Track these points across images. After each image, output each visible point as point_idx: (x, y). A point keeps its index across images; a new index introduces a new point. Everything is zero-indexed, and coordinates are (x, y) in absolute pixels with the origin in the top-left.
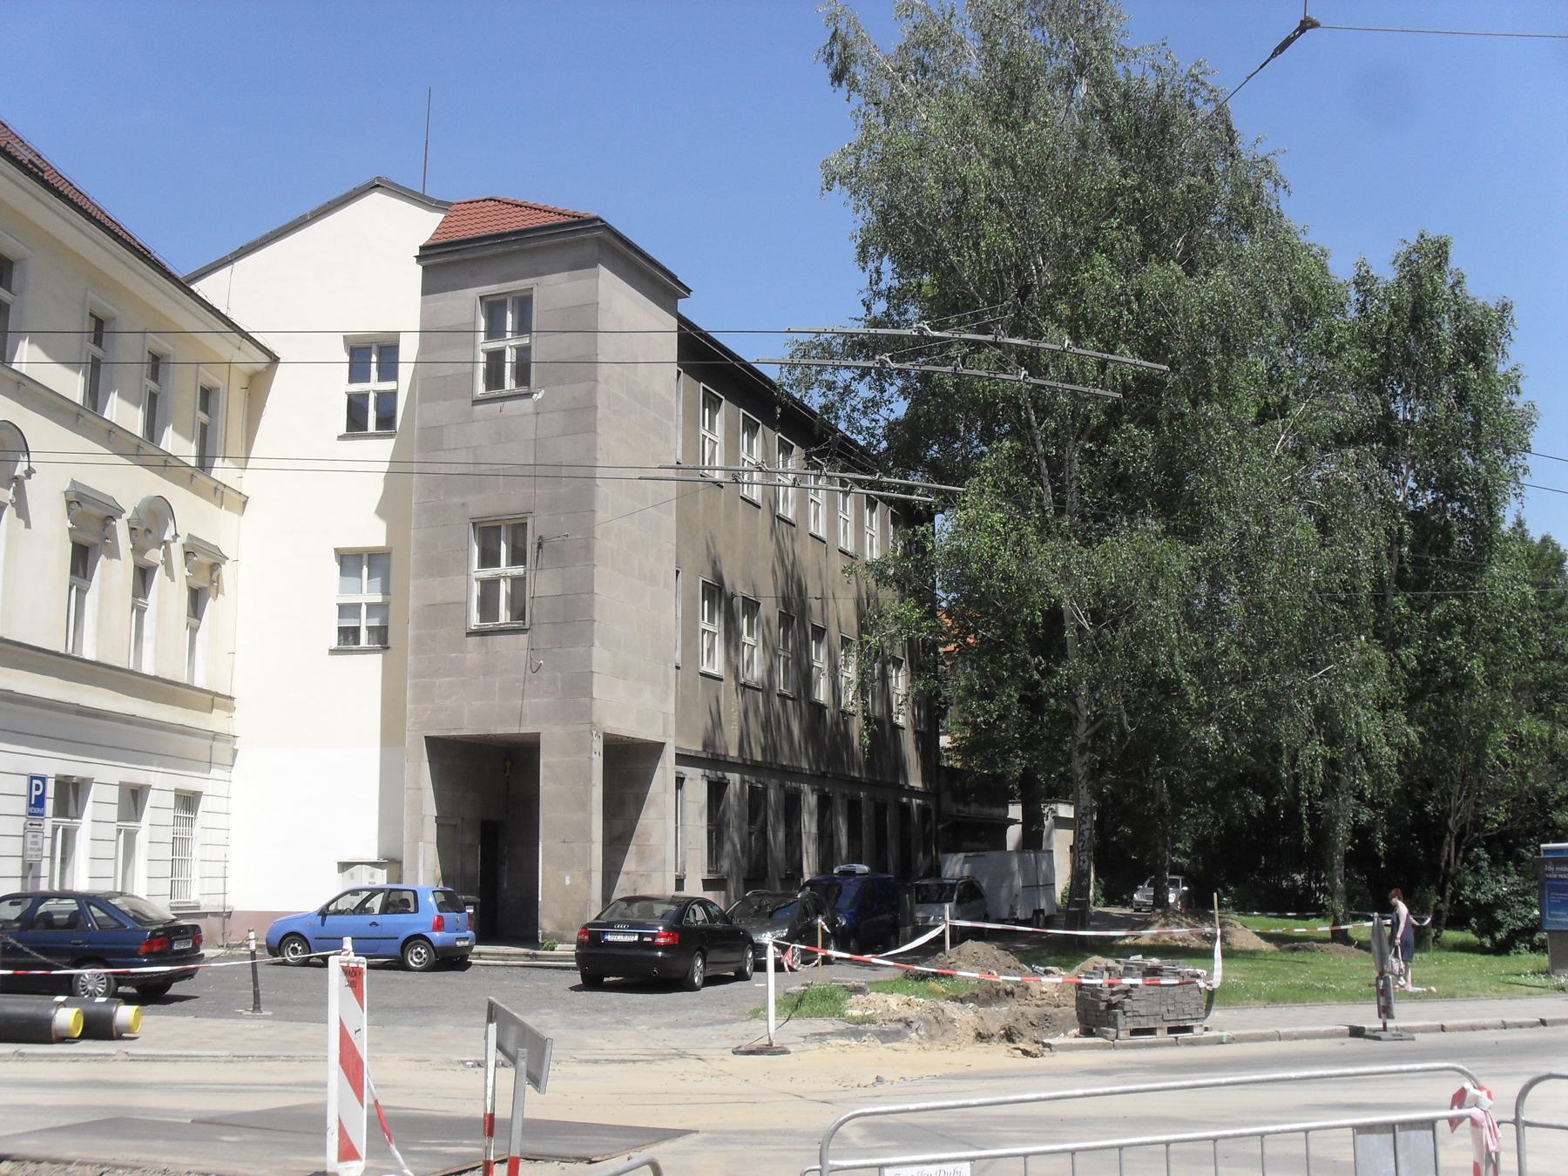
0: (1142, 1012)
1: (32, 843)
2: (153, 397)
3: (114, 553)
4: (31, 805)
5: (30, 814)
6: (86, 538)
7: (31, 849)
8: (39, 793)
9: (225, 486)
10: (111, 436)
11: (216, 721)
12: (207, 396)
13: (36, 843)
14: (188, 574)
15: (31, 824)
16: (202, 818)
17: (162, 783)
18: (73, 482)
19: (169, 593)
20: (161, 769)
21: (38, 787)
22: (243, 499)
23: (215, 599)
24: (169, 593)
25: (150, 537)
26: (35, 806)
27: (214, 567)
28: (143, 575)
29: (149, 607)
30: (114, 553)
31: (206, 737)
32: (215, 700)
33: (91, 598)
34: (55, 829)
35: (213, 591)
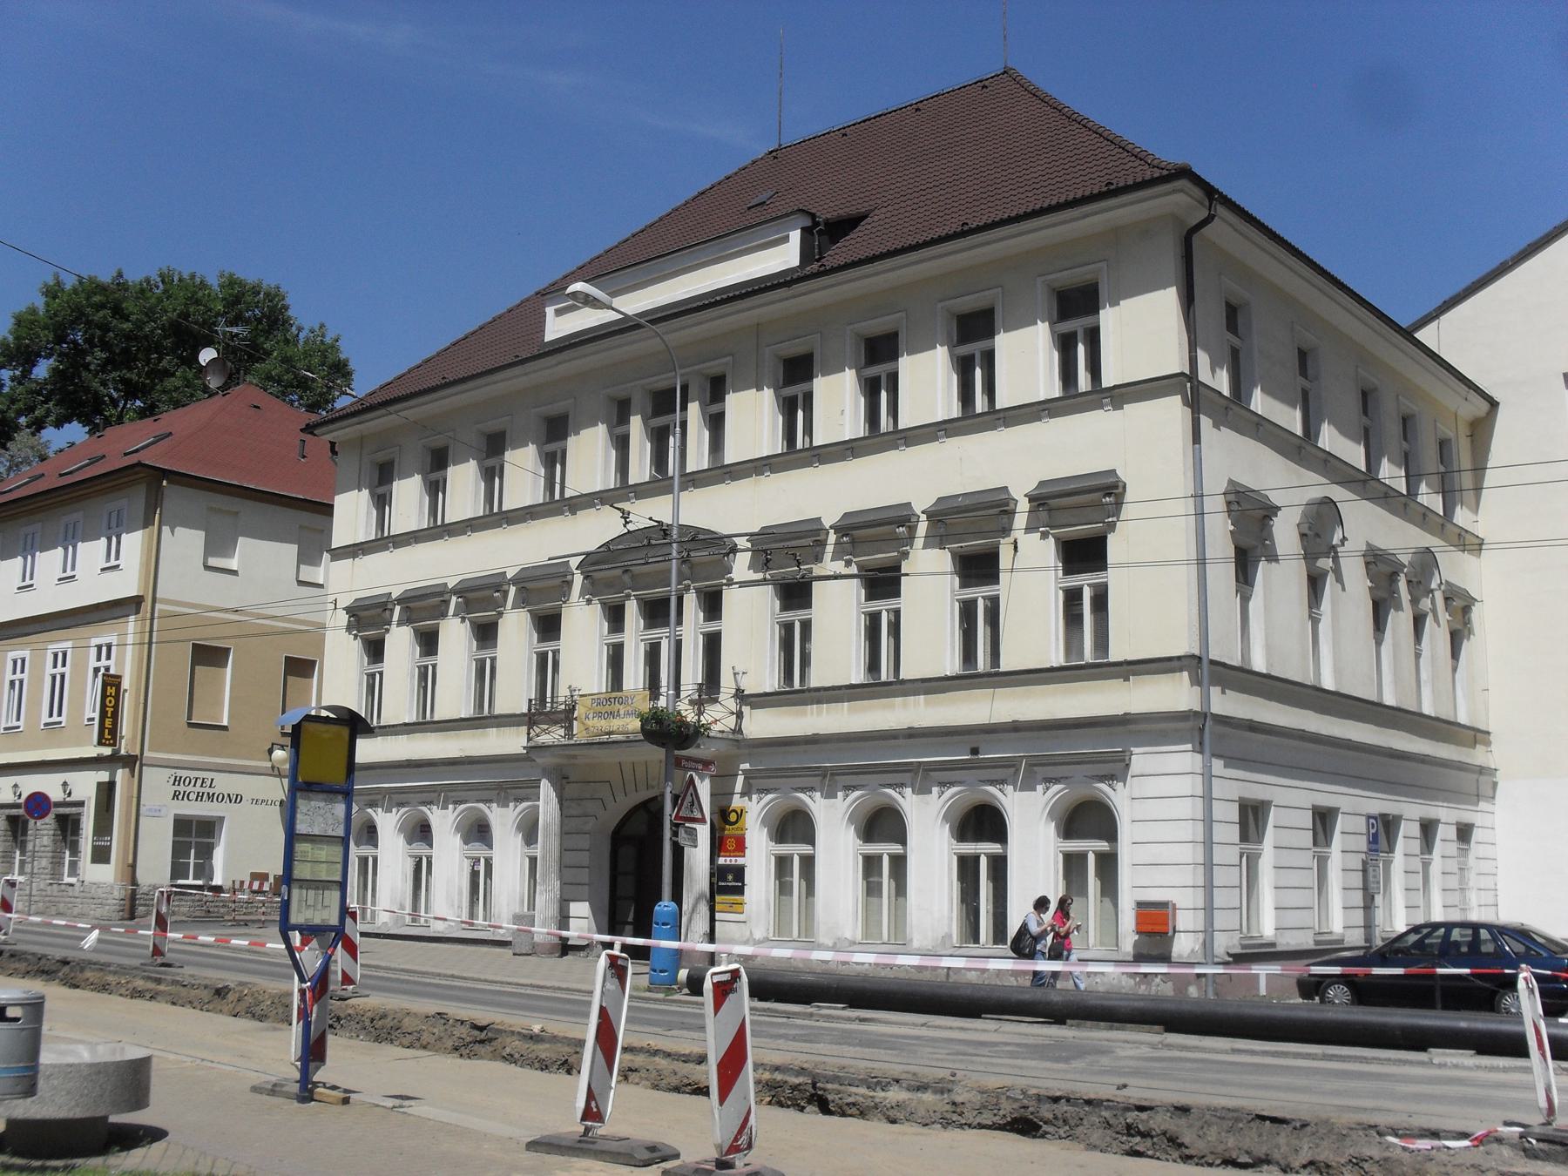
2: (1305, 395)
3: (1399, 607)
4: (1370, 842)
5: (1370, 850)
6: (1247, 542)
9: (1466, 531)
10: (1261, 430)
11: (1478, 756)
12: (1444, 445)
14: (1450, 618)
16: (1475, 849)
17: (1447, 815)
18: (1231, 482)
19: (1437, 635)
20: (1445, 804)
21: (1373, 824)
23: (1469, 639)
24: (1437, 635)
25: (1421, 587)
27: (1466, 610)
28: (1418, 622)
29: (1423, 653)
30: (1399, 607)
31: (1473, 772)
32: (1477, 736)
33: (1255, 604)
35: (1466, 632)
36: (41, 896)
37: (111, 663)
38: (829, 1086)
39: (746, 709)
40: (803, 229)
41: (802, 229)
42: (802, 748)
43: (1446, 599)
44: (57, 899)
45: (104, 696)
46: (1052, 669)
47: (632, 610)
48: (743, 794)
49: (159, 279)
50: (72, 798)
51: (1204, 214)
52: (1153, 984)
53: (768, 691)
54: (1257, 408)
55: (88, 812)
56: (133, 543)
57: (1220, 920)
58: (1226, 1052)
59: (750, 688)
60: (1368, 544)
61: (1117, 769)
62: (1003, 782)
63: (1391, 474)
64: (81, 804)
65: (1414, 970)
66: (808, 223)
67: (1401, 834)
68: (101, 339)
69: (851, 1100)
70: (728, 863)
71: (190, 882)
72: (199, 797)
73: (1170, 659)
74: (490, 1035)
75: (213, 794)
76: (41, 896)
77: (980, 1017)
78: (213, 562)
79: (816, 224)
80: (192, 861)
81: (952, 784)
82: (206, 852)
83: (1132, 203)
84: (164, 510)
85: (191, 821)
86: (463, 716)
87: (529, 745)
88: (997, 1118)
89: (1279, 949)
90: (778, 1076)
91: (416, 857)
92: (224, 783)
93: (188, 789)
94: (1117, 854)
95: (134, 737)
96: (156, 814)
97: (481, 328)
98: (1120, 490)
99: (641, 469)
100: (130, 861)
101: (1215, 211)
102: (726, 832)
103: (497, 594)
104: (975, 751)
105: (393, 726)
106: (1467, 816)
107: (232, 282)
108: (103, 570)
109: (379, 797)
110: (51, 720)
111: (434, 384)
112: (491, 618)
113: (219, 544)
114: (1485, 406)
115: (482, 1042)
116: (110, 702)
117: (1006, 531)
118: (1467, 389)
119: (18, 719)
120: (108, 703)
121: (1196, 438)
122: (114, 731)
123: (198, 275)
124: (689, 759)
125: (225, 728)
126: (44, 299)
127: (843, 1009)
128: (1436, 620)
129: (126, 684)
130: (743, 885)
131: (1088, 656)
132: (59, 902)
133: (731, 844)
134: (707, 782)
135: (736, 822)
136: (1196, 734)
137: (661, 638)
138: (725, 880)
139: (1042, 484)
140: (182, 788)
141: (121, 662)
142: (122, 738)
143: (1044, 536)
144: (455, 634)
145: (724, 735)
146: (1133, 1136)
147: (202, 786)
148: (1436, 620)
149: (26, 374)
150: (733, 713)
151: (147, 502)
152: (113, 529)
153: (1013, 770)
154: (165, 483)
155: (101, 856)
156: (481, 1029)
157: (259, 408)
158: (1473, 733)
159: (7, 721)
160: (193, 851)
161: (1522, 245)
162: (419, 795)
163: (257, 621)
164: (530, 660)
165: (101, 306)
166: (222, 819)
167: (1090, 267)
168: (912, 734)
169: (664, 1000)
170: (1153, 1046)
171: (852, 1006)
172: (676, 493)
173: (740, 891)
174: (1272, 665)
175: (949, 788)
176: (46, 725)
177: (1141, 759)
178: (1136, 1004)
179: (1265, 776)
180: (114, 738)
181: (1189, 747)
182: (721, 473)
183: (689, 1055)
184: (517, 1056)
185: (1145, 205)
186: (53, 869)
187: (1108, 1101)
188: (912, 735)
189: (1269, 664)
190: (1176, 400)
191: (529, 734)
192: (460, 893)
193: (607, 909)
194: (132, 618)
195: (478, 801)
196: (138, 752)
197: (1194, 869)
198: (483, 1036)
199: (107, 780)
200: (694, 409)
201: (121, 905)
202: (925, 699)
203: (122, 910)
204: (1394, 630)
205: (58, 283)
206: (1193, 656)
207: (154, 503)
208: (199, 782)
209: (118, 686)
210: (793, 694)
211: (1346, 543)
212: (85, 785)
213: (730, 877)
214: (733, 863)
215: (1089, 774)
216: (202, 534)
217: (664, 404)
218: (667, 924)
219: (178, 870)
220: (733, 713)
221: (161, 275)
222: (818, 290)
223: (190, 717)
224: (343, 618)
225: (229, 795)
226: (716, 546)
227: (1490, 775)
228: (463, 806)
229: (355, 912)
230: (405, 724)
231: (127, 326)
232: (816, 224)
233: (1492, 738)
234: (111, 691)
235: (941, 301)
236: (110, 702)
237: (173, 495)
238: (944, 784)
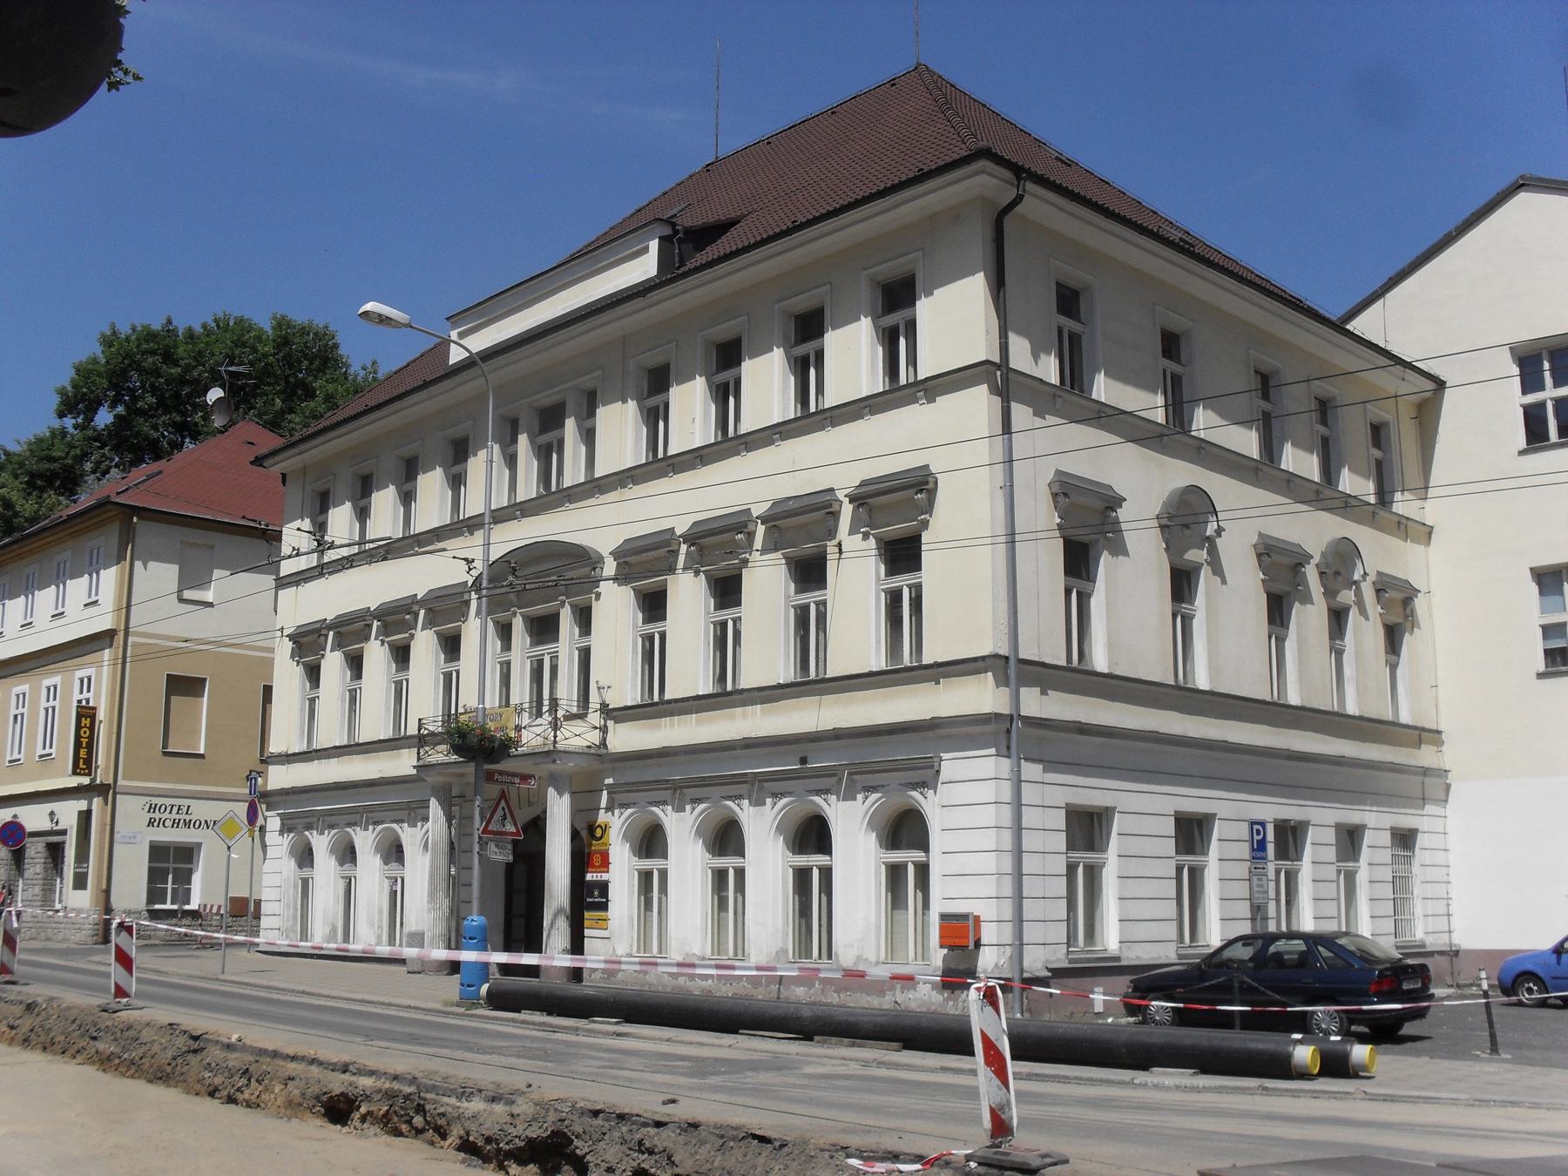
3: (1307, 599)
4: (1253, 850)
5: (1253, 858)
7: (1258, 892)
8: (1260, 837)
9: (1408, 519)
11: (1426, 756)
13: (1262, 886)
14: (1381, 611)
16: (1420, 856)
17: (1377, 822)
19: (1365, 632)
22: (1428, 530)
23: (1412, 633)
24: (1365, 632)
28: (1338, 618)
30: (1307, 599)
31: (1416, 774)
34: (1278, 872)
35: (1408, 625)
36: (34, 922)
37: (90, 695)
38: (429, 1096)
39: (610, 723)
40: (661, 238)
41: (660, 238)
42: (656, 761)
43: (1378, 591)
44: (46, 925)
45: (78, 727)
46: (871, 674)
47: (518, 625)
48: (608, 809)
49: (214, 325)
50: (60, 827)
51: (1013, 194)
52: (960, 1000)
53: (629, 704)
54: (1099, 395)
55: (71, 840)
56: (110, 577)
57: (1031, 933)
58: (933, 1070)
59: (615, 702)
60: (1260, 535)
61: (927, 777)
62: (827, 791)
63: (1299, 461)
64: (64, 832)
66: (667, 231)
68: (152, 385)
69: (441, 1110)
70: (595, 879)
71: (168, 906)
72: (175, 823)
73: (975, 660)
74: (202, 1044)
75: (190, 821)
76: (34, 922)
77: (737, 1033)
78: (188, 594)
79: (676, 232)
80: (169, 886)
81: (783, 795)
82: (184, 878)
83: (940, 188)
84: (136, 547)
85: (169, 848)
86: (382, 738)
87: (419, 764)
88: (542, 1130)
89: (1123, 963)
90: (396, 1086)
91: (390, 878)
92: (201, 810)
93: (164, 816)
94: (929, 865)
95: (107, 767)
96: (131, 840)
97: (422, 355)
98: (931, 486)
99: (528, 488)
100: (104, 887)
101: (1024, 191)
102: (593, 848)
103: (408, 617)
104: (803, 761)
105: (326, 749)
106: (1406, 820)
107: (281, 324)
108: (85, 605)
109: (314, 819)
110: (44, 752)
111: (355, 413)
112: (404, 641)
113: (193, 578)
114: (1430, 385)
115: (195, 1051)
116: (85, 733)
117: (832, 533)
118: (1403, 369)
119: (20, 753)
121: (1007, 428)
122: (88, 761)
124: (501, 773)
125: (202, 756)
126: (102, 348)
127: (617, 1023)
128: (1363, 611)
129: (101, 715)
130: (608, 901)
131: (907, 660)
132: (47, 928)
133: (597, 860)
134: (566, 798)
135: (601, 837)
136: (1003, 737)
137: (544, 655)
138: (592, 896)
139: (863, 484)
140: (157, 815)
141: (97, 696)
142: (97, 767)
143: (866, 536)
144: (376, 654)
145: (592, 751)
146: (643, 1153)
147: (178, 813)
148: (1363, 611)
149: (89, 420)
150: (596, 728)
151: (120, 537)
152: (93, 567)
153: (835, 779)
154: (135, 519)
155: (80, 882)
156: (196, 1038)
157: (253, 444)
158: (1417, 732)
159: (12, 753)
160: (170, 876)
161: (1467, 214)
162: (345, 817)
163: (218, 649)
164: (437, 680)
165: (153, 353)
166: (199, 845)
167: (905, 258)
168: (749, 744)
169: (463, 1015)
170: (866, 1063)
171: (628, 1021)
172: (487, 511)
173: (604, 907)
174: (1117, 664)
175: (781, 799)
176: (41, 756)
177: (952, 765)
178: (879, 1019)
180: (89, 767)
181: (993, 751)
182: (596, 486)
183: (336, 1064)
184: (213, 1065)
185: (952, 189)
186: (44, 895)
187: (638, 1115)
188: (749, 745)
189: (1111, 660)
190: (983, 389)
191: (418, 753)
192: (380, 911)
193: (502, 927)
194: (107, 650)
195: (392, 822)
196: (111, 781)
197: (998, 879)
198: (196, 1046)
199: (85, 809)
200: (570, 424)
201: (95, 930)
202: (762, 710)
203: (97, 935)
204: (1298, 624)
205: (114, 333)
206: (996, 656)
207: (128, 536)
208: (175, 809)
209: (93, 718)
210: (653, 708)
211: (1223, 533)
212: (68, 813)
213: (596, 893)
214: (599, 878)
215: (903, 782)
216: (175, 568)
217: (551, 419)
218: (475, 939)
219: (155, 895)
220: (596, 728)
221: (216, 321)
222: (669, 298)
223: (165, 745)
224: (288, 645)
225: (206, 822)
226: (582, 558)
227: (1439, 776)
228: (380, 827)
229: (132, 927)
230: (336, 747)
231: (176, 371)
232: (676, 232)
233: (1444, 736)
234: (86, 722)
235: (778, 301)
237: (146, 532)
238: (776, 795)
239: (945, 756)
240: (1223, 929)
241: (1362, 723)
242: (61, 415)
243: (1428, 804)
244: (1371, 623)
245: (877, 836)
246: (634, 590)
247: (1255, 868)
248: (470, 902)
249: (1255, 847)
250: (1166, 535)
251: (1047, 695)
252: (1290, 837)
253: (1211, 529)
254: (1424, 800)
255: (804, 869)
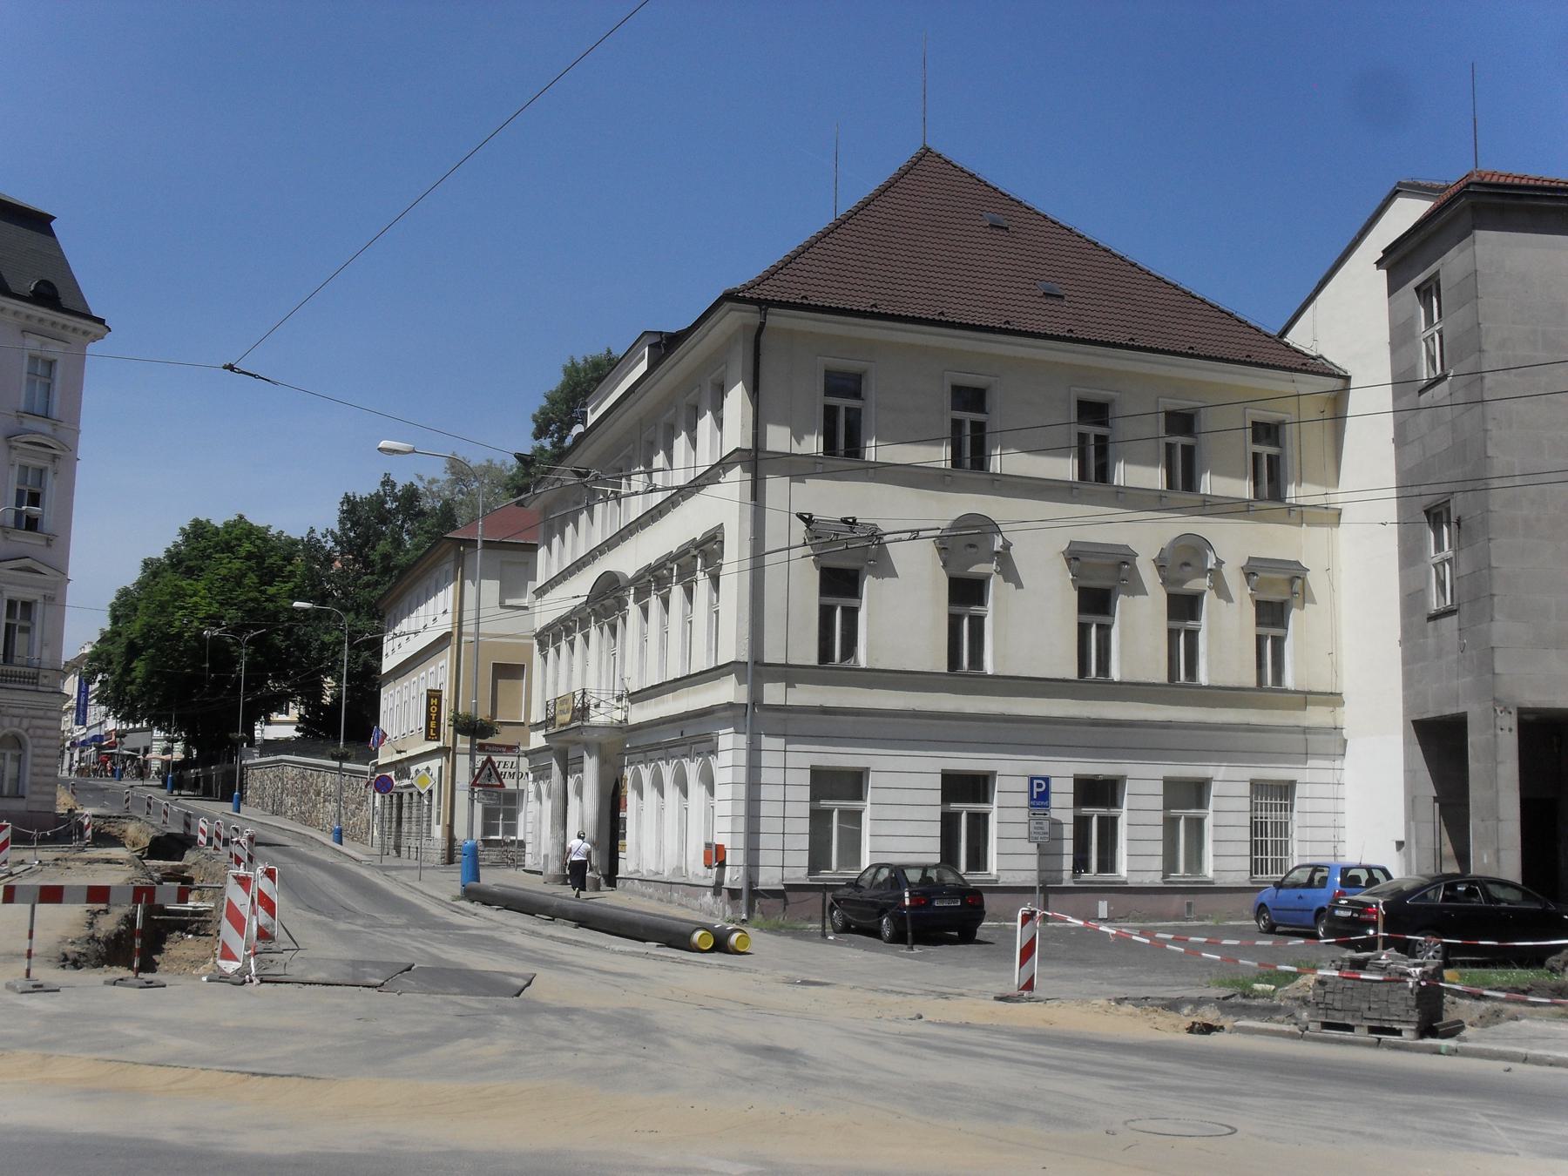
0: (1338, 1005)
1: (1035, 828)
3: (1137, 588)
5: (1032, 806)
15: (1034, 814)
22: (1336, 512)
26: (1037, 800)
30: (1137, 588)
32: (1333, 699)
35: (1295, 602)
40: (650, 346)
65: (1347, 939)
67: (1126, 793)
78: (508, 602)
100: (448, 823)
116: (434, 710)
120: (431, 710)
123: (589, 357)
124: (491, 745)
129: (445, 695)
147: (504, 767)
150: (619, 708)
154: (462, 548)
173: (625, 838)
179: (841, 748)
181: (732, 730)
193: (608, 852)
196: (451, 745)
208: (502, 765)
219: (489, 828)
236: (434, 709)
239: (721, 732)
240: (871, 858)
241: (1213, 691)
242: (537, 437)
243: (1311, 759)
244: (1234, 606)
245: (707, 787)
246: (641, 608)
247: (1034, 814)
248: (1299, 856)
249: (1035, 797)
250: (943, 555)
251: (795, 687)
252: (1197, 792)
253: (998, 543)
254: (1307, 755)
255: (1103, 817)
